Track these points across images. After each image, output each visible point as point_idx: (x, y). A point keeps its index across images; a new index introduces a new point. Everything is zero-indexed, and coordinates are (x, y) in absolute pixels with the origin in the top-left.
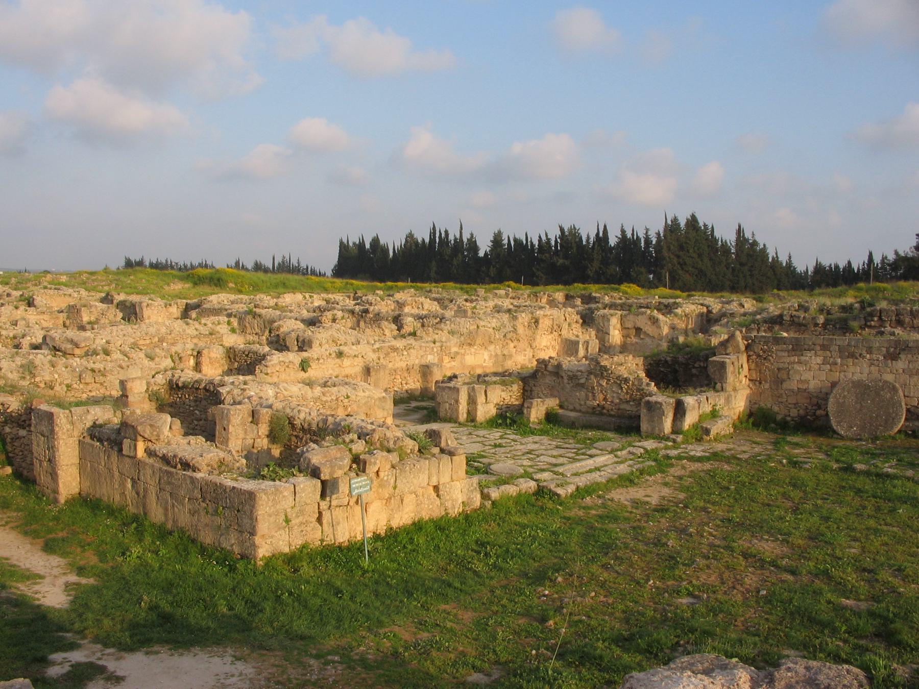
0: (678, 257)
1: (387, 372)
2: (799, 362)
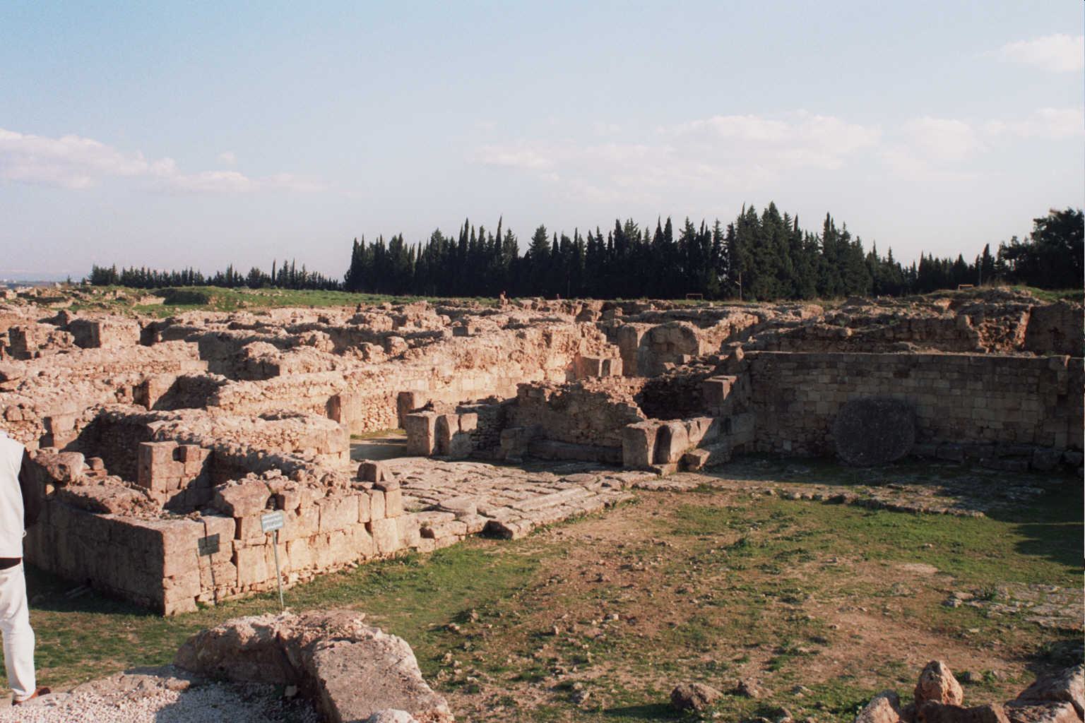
0: (755, 254)
1: (360, 400)
2: (805, 382)
